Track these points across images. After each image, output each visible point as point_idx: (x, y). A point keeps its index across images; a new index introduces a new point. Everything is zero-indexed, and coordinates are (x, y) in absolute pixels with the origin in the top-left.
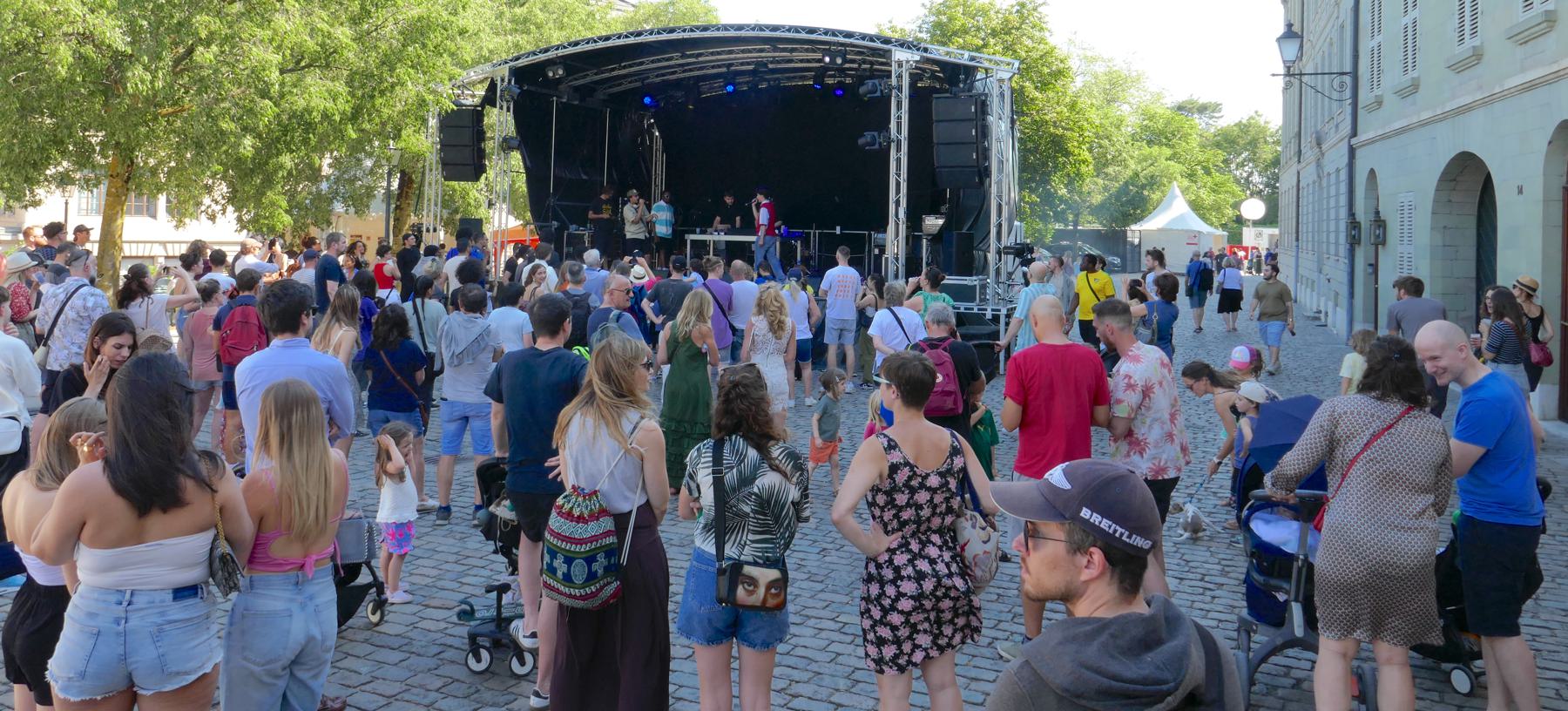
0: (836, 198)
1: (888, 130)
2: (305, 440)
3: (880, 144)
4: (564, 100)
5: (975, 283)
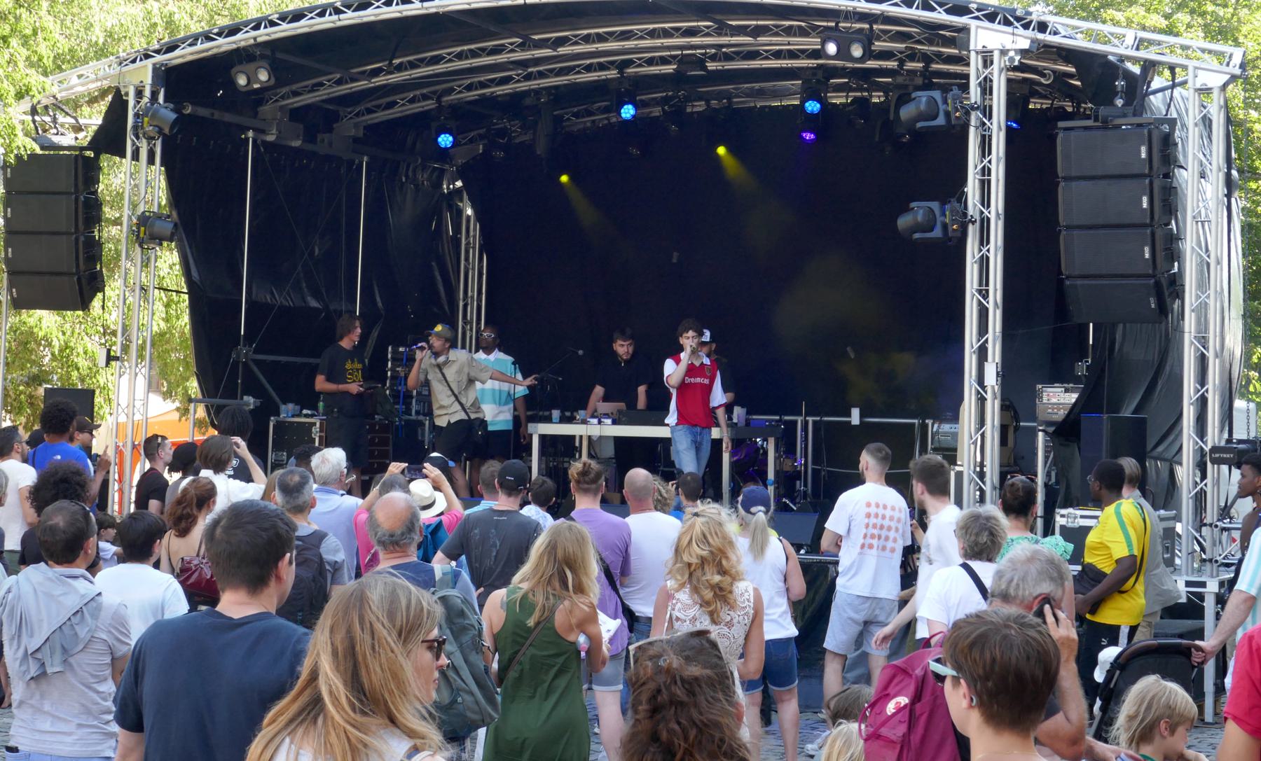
1: (961, 197)
3: (945, 226)
4: (271, 138)
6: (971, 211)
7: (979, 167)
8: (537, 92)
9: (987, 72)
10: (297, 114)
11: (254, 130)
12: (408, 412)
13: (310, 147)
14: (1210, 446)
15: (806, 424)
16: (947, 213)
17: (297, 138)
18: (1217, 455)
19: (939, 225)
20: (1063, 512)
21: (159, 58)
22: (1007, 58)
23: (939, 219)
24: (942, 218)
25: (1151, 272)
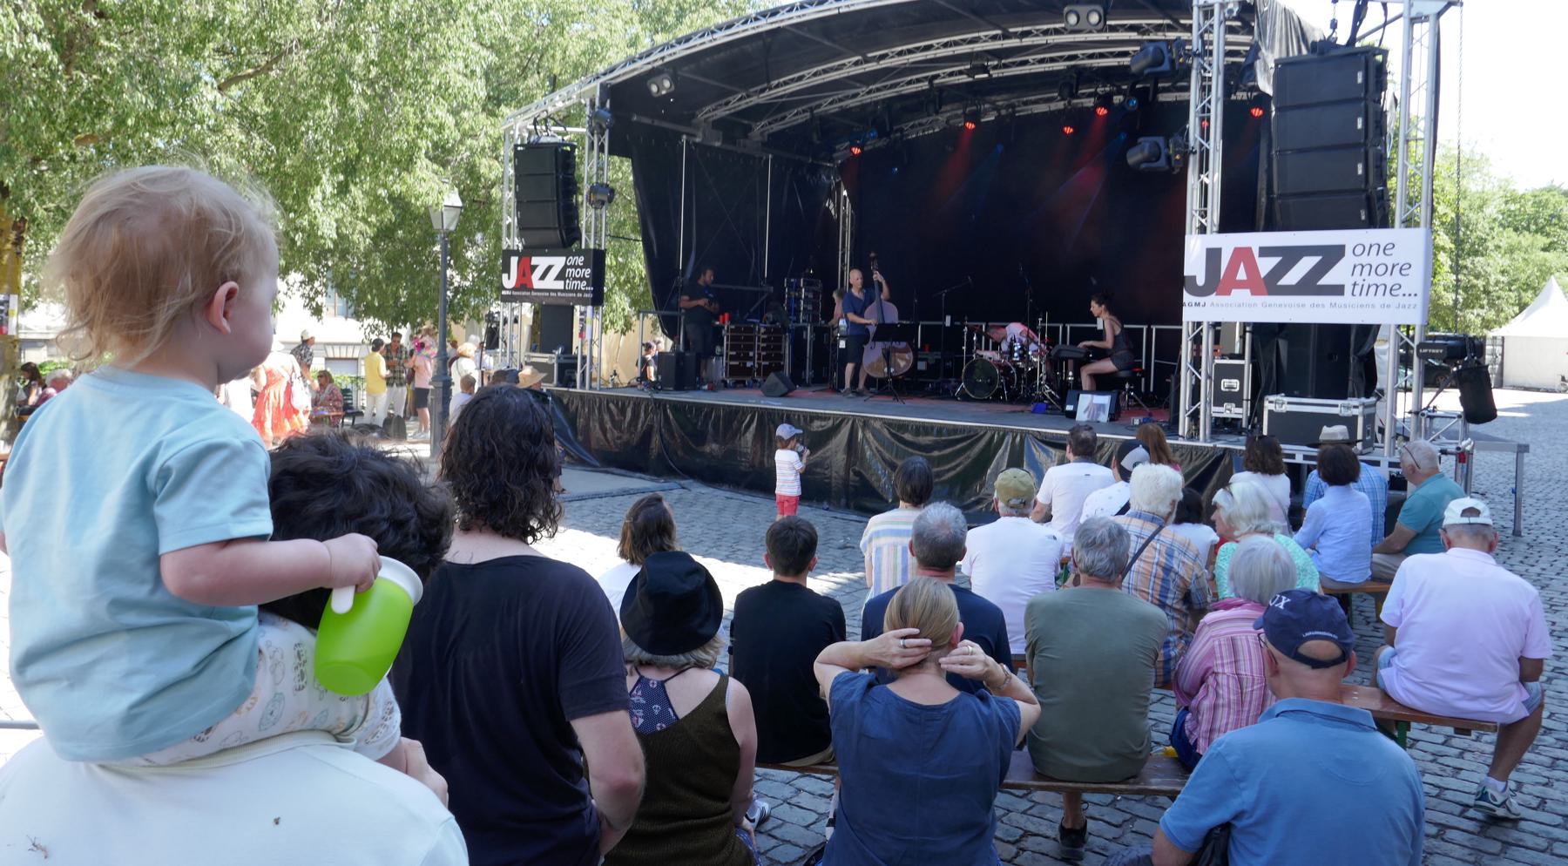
0: (1094, 282)
1: (1184, 133)
2: (984, 728)
3: (1169, 158)
4: (698, 140)
5: (1355, 412)
6: (1192, 143)
7: (1200, 106)
8: (876, 103)
9: (1208, 23)
10: (719, 124)
11: (688, 134)
12: (797, 321)
13: (730, 147)
14: (1417, 341)
15: (1065, 329)
16: (1171, 146)
17: (718, 140)
18: (1425, 351)
19: (1163, 158)
20: (1272, 398)
21: (603, 79)
22: (1226, 11)
23: (1164, 151)
24: (1166, 150)
25: (1363, 186)
